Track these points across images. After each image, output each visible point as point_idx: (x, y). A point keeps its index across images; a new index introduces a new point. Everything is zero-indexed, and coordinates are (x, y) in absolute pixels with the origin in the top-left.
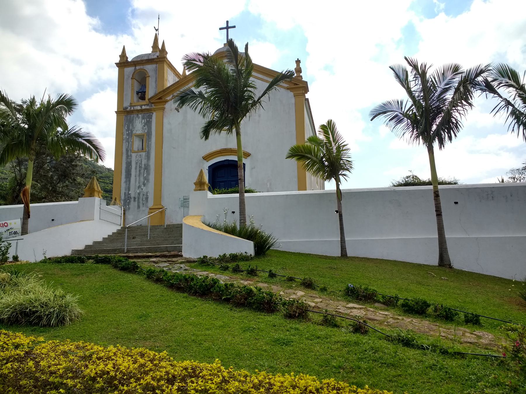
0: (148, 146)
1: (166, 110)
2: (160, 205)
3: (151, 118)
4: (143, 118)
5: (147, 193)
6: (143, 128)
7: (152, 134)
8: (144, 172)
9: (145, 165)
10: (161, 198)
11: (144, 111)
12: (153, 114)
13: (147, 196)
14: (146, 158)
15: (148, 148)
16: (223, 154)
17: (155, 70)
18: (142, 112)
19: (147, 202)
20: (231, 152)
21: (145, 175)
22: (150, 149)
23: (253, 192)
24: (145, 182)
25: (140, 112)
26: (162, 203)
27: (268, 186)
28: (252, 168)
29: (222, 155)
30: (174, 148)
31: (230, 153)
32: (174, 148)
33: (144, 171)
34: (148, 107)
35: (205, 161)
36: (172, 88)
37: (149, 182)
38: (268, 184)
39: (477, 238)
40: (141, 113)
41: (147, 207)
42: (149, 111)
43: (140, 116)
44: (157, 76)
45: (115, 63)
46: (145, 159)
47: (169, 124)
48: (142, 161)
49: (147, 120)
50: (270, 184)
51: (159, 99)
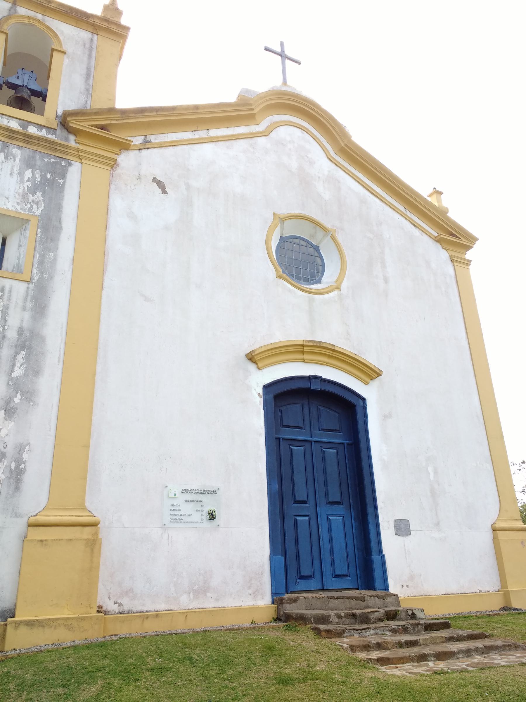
0: (41, 262)
1: (118, 171)
2: (83, 508)
3: (63, 176)
4: (29, 164)
5: (20, 449)
6: (24, 196)
7: (61, 228)
8: (15, 358)
9: (20, 331)
10: (85, 478)
11: (38, 145)
12: (70, 164)
13: (19, 461)
14: (29, 305)
15: (42, 271)
16: (306, 357)
17: (88, 46)
18: (28, 143)
19: (17, 488)
20: (330, 357)
21: (18, 372)
22: (51, 277)
23: (14, 23)
24: (17, 400)
25: (17, 139)
26: (87, 498)
27: (432, 476)
28: (386, 417)
29: (304, 361)
30: (147, 299)
31: (326, 359)
32: (147, 299)
33: (17, 353)
34: (51, 137)
35: (252, 367)
36: (149, 116)
37: (35, 404)
38: (430, 469)
39: (102, 130)
40: (21, 144)
41: (17, 515)
42: (56, 150)
43: (16, 152)
44: (93, 63)
45: (167, 193)
46: (24, 309)
47: (132, 216)
48: (11, 312)
49: (43, 177)
50: (436, 472)
51: (102, 128)
